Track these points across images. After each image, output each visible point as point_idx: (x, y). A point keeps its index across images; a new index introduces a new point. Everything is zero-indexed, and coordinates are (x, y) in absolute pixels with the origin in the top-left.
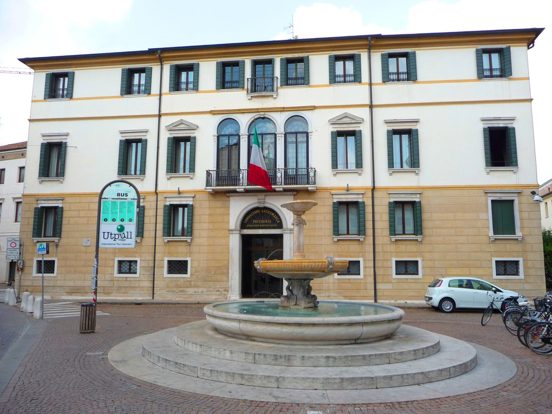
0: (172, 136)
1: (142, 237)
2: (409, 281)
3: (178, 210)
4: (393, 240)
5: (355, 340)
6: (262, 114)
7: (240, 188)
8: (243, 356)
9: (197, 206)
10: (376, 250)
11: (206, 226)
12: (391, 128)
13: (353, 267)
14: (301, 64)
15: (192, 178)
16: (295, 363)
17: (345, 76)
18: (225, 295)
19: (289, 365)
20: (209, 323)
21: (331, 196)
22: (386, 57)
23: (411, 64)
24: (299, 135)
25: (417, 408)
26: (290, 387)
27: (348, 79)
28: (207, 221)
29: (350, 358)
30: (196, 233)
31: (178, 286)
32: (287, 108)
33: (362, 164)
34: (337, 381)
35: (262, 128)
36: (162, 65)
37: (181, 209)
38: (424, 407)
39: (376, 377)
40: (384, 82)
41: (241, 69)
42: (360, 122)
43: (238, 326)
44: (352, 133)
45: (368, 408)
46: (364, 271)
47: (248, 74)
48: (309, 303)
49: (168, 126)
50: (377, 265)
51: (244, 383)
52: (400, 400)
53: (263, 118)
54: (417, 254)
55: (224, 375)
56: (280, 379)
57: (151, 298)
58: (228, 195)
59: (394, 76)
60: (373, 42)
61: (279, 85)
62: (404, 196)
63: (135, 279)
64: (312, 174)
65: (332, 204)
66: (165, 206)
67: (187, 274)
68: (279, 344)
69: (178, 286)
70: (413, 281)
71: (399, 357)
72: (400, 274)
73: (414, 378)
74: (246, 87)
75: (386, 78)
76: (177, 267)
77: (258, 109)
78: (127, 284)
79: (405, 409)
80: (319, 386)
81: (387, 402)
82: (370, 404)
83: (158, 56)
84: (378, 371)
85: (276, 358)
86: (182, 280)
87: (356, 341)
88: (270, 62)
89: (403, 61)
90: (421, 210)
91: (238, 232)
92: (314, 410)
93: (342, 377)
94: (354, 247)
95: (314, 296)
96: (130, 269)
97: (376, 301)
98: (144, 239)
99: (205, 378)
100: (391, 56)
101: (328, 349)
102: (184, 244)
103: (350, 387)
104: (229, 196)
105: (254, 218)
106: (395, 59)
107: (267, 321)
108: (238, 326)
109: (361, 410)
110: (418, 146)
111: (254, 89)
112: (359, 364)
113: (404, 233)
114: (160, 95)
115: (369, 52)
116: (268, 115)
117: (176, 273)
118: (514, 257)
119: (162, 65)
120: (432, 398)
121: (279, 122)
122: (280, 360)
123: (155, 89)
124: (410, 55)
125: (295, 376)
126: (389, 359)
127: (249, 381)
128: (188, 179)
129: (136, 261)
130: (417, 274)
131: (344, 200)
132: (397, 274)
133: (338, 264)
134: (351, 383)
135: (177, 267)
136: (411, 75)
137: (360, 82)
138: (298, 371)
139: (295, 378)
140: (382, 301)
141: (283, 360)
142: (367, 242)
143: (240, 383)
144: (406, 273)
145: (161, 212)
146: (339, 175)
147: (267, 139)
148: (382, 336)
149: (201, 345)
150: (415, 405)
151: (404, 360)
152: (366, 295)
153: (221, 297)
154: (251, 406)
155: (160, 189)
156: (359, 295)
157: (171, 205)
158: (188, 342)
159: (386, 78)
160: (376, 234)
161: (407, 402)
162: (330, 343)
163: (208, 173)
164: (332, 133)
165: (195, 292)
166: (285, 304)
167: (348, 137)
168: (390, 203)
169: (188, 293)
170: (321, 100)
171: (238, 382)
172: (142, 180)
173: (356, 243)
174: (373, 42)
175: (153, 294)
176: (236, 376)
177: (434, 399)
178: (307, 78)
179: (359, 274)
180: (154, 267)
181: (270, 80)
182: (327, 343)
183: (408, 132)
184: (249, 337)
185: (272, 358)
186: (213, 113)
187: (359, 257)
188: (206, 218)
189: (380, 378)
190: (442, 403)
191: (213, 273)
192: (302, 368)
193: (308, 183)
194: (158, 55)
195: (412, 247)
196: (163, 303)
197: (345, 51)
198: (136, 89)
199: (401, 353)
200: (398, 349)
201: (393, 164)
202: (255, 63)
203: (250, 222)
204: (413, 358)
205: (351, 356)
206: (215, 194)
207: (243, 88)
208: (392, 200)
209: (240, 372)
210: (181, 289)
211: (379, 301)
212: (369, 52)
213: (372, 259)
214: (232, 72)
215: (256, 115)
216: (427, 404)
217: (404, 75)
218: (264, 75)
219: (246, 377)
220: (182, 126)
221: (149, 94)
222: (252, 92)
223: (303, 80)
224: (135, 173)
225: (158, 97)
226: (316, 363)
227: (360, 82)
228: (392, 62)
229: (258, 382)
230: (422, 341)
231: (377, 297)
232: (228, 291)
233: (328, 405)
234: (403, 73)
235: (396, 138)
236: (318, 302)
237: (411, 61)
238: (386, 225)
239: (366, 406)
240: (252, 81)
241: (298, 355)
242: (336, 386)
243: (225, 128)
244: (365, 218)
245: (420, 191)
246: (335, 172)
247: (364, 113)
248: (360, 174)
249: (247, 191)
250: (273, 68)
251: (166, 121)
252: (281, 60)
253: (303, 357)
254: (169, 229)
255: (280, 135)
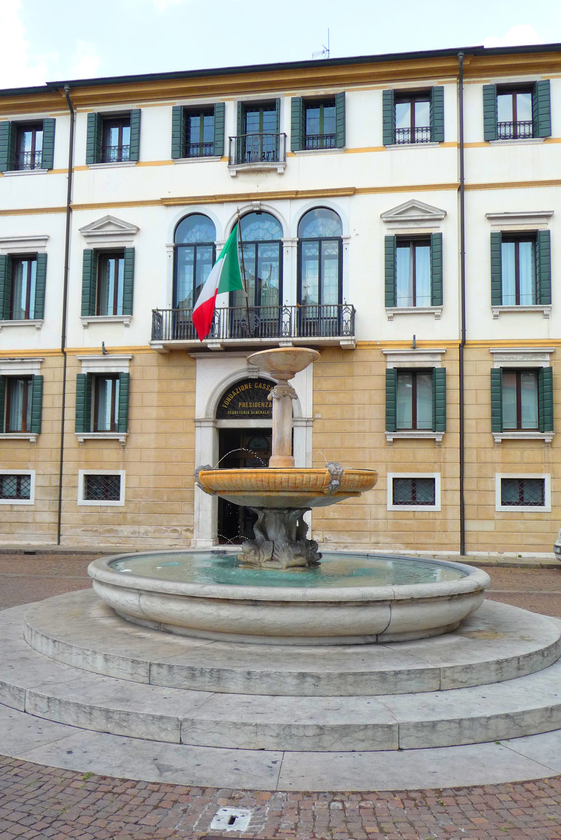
0: (92, 247)
1: (39, 432)
2: (527, 516)
3: (105, 384)
4: (498, 439)
5: (377, 635)
6: (255, 205)
7: (212, 343)
8: (128, 667)
9: (136, 375)
10: (466, 459)
11: (153, 412)
12: (498, 229)
13: (413, 490)
14: (331, 108)
15: (127, 325)
16: (232, 686)
17: (413, 130)
18: (187, 538)
19: (220, 689)
20: (98, 597)
21: (383, 358)
22: (491, 92)
23: (541, 105)
24: (324, 244)
25: (479, 807)
26: (206, 742)
27: (419, 136)
28: (155, 404)
29: (350, 679)
30: (135, 425)
31: (102, 522)
32: (303, 192)
33: (442, 298)
34: (310, 732)
35: (255, 231)
36: (72, 113)
37: (109, 382)
38: (496, 805)
39: (399, 726)
40: (487, 141)
41: (218, 120)
42: (439, 217)
43: (136, 602)
44: (424, 240)
45: (363, 804)
46: (443, 497)
47: (231, 128)
48: (297, 556)
49: (84, 228)
50: (466, 487)
51: (110, 730)
52: (441, 786)
53: (259, 212)
54: (543, 466)
55: (72, 709)
56: (185, 725)
57: (56, 543)
58: (193, 355)
59: (508, 129)
60: (467, 63)
61: (288, 150)
62: (519, 357)
63: (27, 508)
64: (346, 316)
65: (384, 372)
66: (79, 376)
67: (118, 499)
68: (217, 641)
69: (102, 522)
70: (534, 516)
71: (463, 677)
72: (509, 504)
73: (486, 727)
74: (227, 154)
75: (492, 132)
76: (102, 487)
77: (248, 195)
78: (13, 517)
79: (450, 810)
80: (268, 741)
81: (410, 788)
82: (369, 793)
83: (64, 96)
84: (408, 709)
85: (192, 673)
86: (109, 510)
87: (379, 638)
88: (272, 106)
89: (524, 100)
90: (551, 384)
91: (211, 424)
92: (237, 807)
93: (321, 723)
94: (424, 453)
95: (313, 543)
96: (18, 490)
97: (463, 552)
98: (43, 437)
99: (38, 714)
100: (502, 89)
101: (313, 656)
102: (113, 445)
103: (338, 746)
104: (195, 359)
105: (239, 398)
106: (510, 96)
107: (189, 593)
108: (136, 602)
109: (344, 809)
110: (549, 263)
111: (243, 156)
112: (370, 691)
113: (519, 428)
114: (71, 171)
115: (461, 83)
116: (267, 206)
117: (99, 499)
118: (418, 471)
119: (72, 113)
120: (519, 779)
121: (287, 219)
122: (201, 679)
123: (60, 159)
124: (539, 88)
125: (218, 719)
126: (439, 681)
127: (121, 727)
128: (121, 328)
129: (29, 476)
130: (542, 504)
131: (407, 365)
132: (503, 504)
133: (352, 477)
134: (342, 736)
135: (102, 487)
136: (540, 128)
137: (442, 141)
138: (234, 706)
139: (217, 723)
140: (475, 553)
141: (207, 679)
142: (447, 445)
143: (104, 728)
144: (521, 502)
145: (72, 387)
146: (398, 319)
147: (264, 251)
148: (436, 628)
149: (54, 641)
150: (475, 799)
151: (474, 682)
152: (446, 541)
153: (180, 542)
154: (95, 791)
155: (69, 345)
156: (432, 541)
157: (90, 375)
158: (37, 633)
159: (492, 132)
160: (466, 430)
161: (459, 789)
162: (322, 641)
163: (157, 316)
164: (387, 239)
165: (134, 533)
166: (251, 558)
167: (417, 248)
168: (493, 371)
169: (120, 535)
170: (368, 173)
171: (99, 728)
172: (39, 329)
173: (429, 445)
174: (466, 61)
175: (59, 535)
176: (96, 713)
177: (522, 783)
178: (341, 136)
179: (433, 503)
180: (61, 486)
181: (273, 140)
182: (315, 641)
183: (531, 237)
184: (162, 626)
185: (185, 673)
186: (167, 203)
187: (433, 471)
188: (153, 399)
189: (408, 726)
190: (541, 793)
191: (165, 498)
192: (245, 698)
193: (339, 333)
194: (64, 94)
195: (533, 454)
196: (75, 552)
197: (413, 80)
198: (27, 159)
199: (467, 668)
200: (462, 660)
201: (501, 298)
202: (245, 108)
203: (233, 406)
204: (494, 678)
205: (355, 674)
206: (170, 353)
207: (222, 155)
208: (497, 366)
209: (104, 706)
210: (108, 527)
211: (469, 553)
212: (461, 83)
213: (458, 475)
214: (202, 126)
215: (244, 207)
216: (504, 797)
217: (527, 127)
218: (261, 129)
219: (116, 717)
220: (110, 229)
221: (51, 169)
222: (238, 162)
223: (334, 140)
224: (27, 316)
225: (67, 175)
226: (276, 688)
227: (442, 141)
228: (504, 101)
229: (139, 729)
230: (523, 638)
231: (467, 546)
232: (192, 532)
233: (273, 792)
234: (525, 123)
235: (508, 249)
236: (320, 555)
237: (540, 99)
238: (485, 412)
239: (359, 798)
240: (238, 142)
241: (238, 670)
242: (307, 744)
243: (190, 233)
244: (445, 399)
245: (550, 348)
246: (391, 314)
247: (448, 201)
248: (438, 317)
249: (227, 349)
250: (278, 116)
251: (81, 219)
252: (294, 101)
253: (249, 673)
254: (88, 419)
255: (290, 244)
